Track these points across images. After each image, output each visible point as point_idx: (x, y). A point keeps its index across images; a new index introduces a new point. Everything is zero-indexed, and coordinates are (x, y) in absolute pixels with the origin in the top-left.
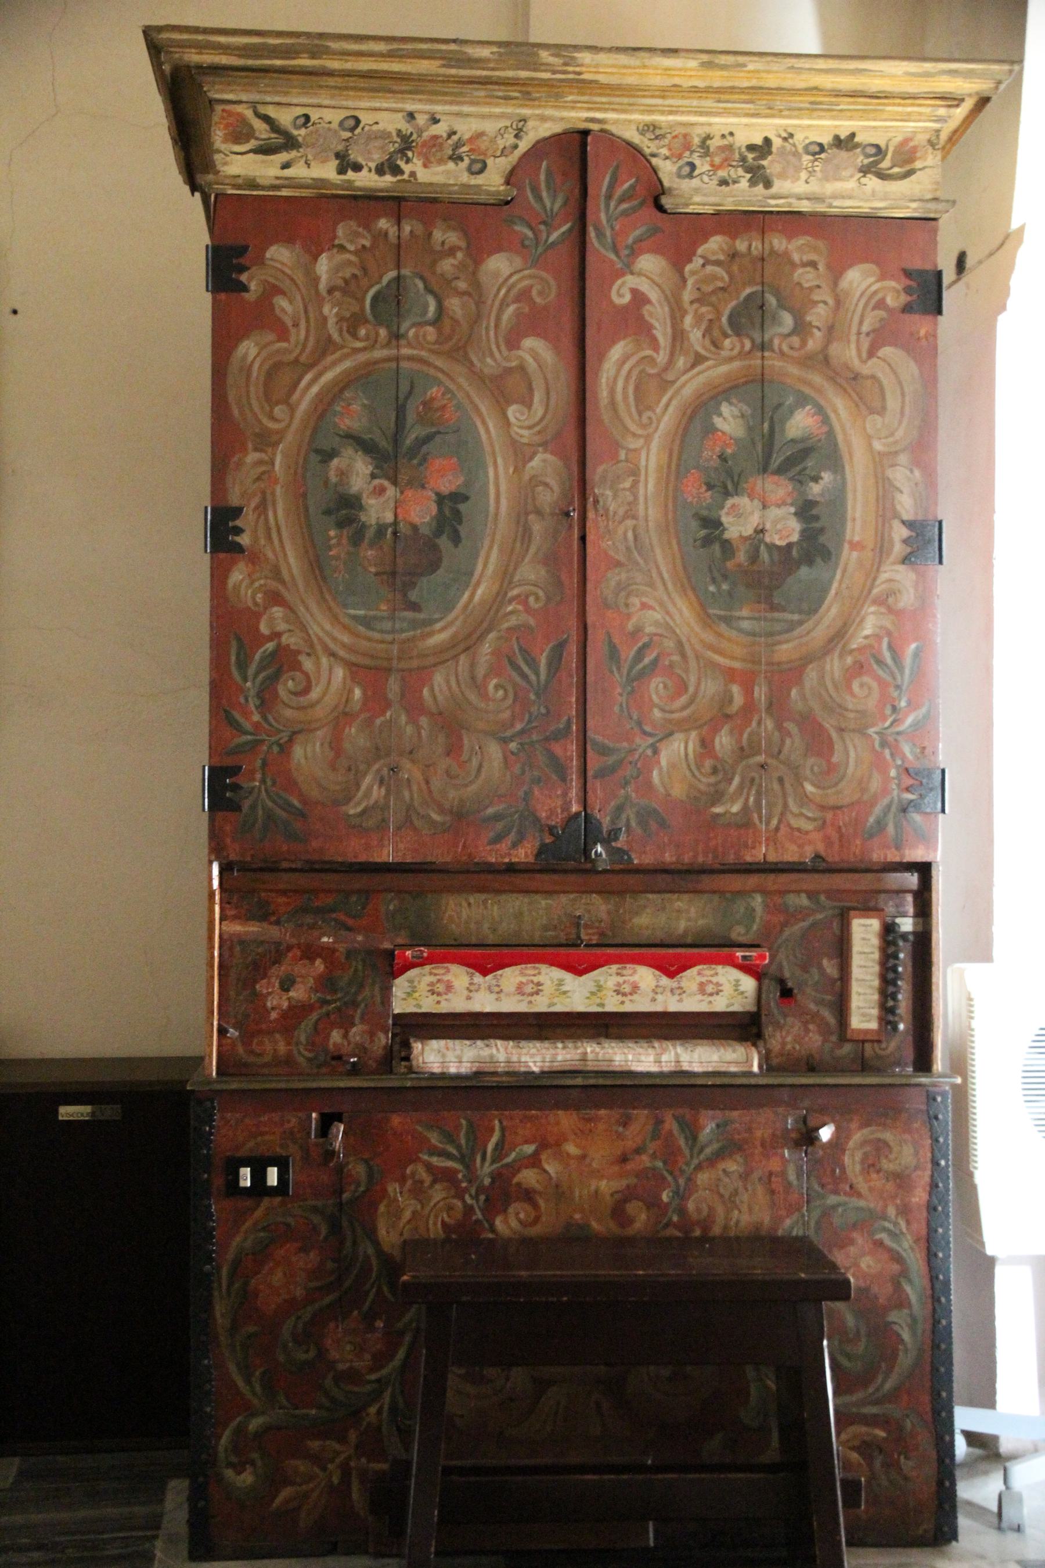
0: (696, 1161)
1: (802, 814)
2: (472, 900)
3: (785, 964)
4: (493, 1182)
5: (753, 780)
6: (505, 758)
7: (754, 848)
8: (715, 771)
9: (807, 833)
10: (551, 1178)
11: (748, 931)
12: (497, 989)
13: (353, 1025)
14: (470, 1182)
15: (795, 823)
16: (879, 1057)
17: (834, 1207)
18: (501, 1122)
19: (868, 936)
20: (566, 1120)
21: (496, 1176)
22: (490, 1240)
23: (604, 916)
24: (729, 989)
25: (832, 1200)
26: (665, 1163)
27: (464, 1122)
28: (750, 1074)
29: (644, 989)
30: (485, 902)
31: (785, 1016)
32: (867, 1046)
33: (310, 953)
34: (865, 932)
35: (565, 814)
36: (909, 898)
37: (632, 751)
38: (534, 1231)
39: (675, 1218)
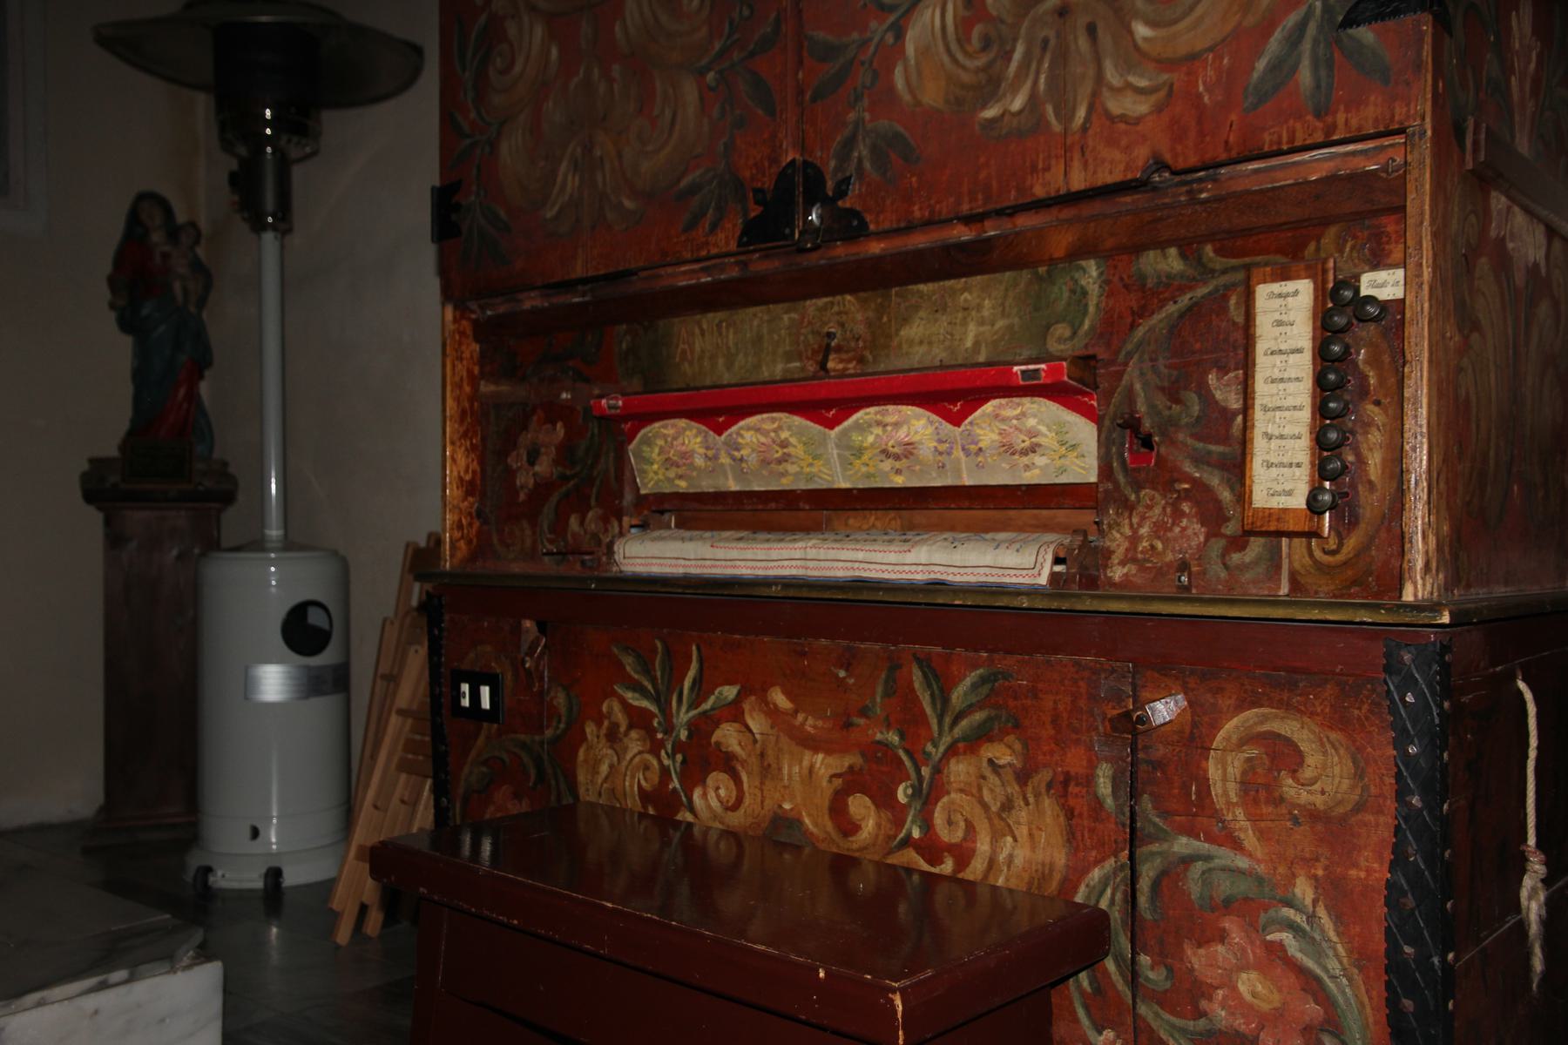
0: (946, 740)
1: (1129, 86)
3: (1138, 386)
4: (690, 736)
5: (1046, 41)
6: (702, 99)
8: (987, 44)
9: (1139, 120)
10: (755, 741)
11: (1074, 333)
13: (589, 508)
14: (665, 733)
15: (1115, 106)
17: (1187, 861)
18: (698, 649)
21: (692, 726)
22: (690, 825)
23: (860, 329)
25: (1183, 845)
26: (902, 737)
27: (659, 644)
30: (719, 326)
31: (1138, 487)
33: (555, 412)
37: (865, 43)
38: (736, 819)
39: (916, 834)
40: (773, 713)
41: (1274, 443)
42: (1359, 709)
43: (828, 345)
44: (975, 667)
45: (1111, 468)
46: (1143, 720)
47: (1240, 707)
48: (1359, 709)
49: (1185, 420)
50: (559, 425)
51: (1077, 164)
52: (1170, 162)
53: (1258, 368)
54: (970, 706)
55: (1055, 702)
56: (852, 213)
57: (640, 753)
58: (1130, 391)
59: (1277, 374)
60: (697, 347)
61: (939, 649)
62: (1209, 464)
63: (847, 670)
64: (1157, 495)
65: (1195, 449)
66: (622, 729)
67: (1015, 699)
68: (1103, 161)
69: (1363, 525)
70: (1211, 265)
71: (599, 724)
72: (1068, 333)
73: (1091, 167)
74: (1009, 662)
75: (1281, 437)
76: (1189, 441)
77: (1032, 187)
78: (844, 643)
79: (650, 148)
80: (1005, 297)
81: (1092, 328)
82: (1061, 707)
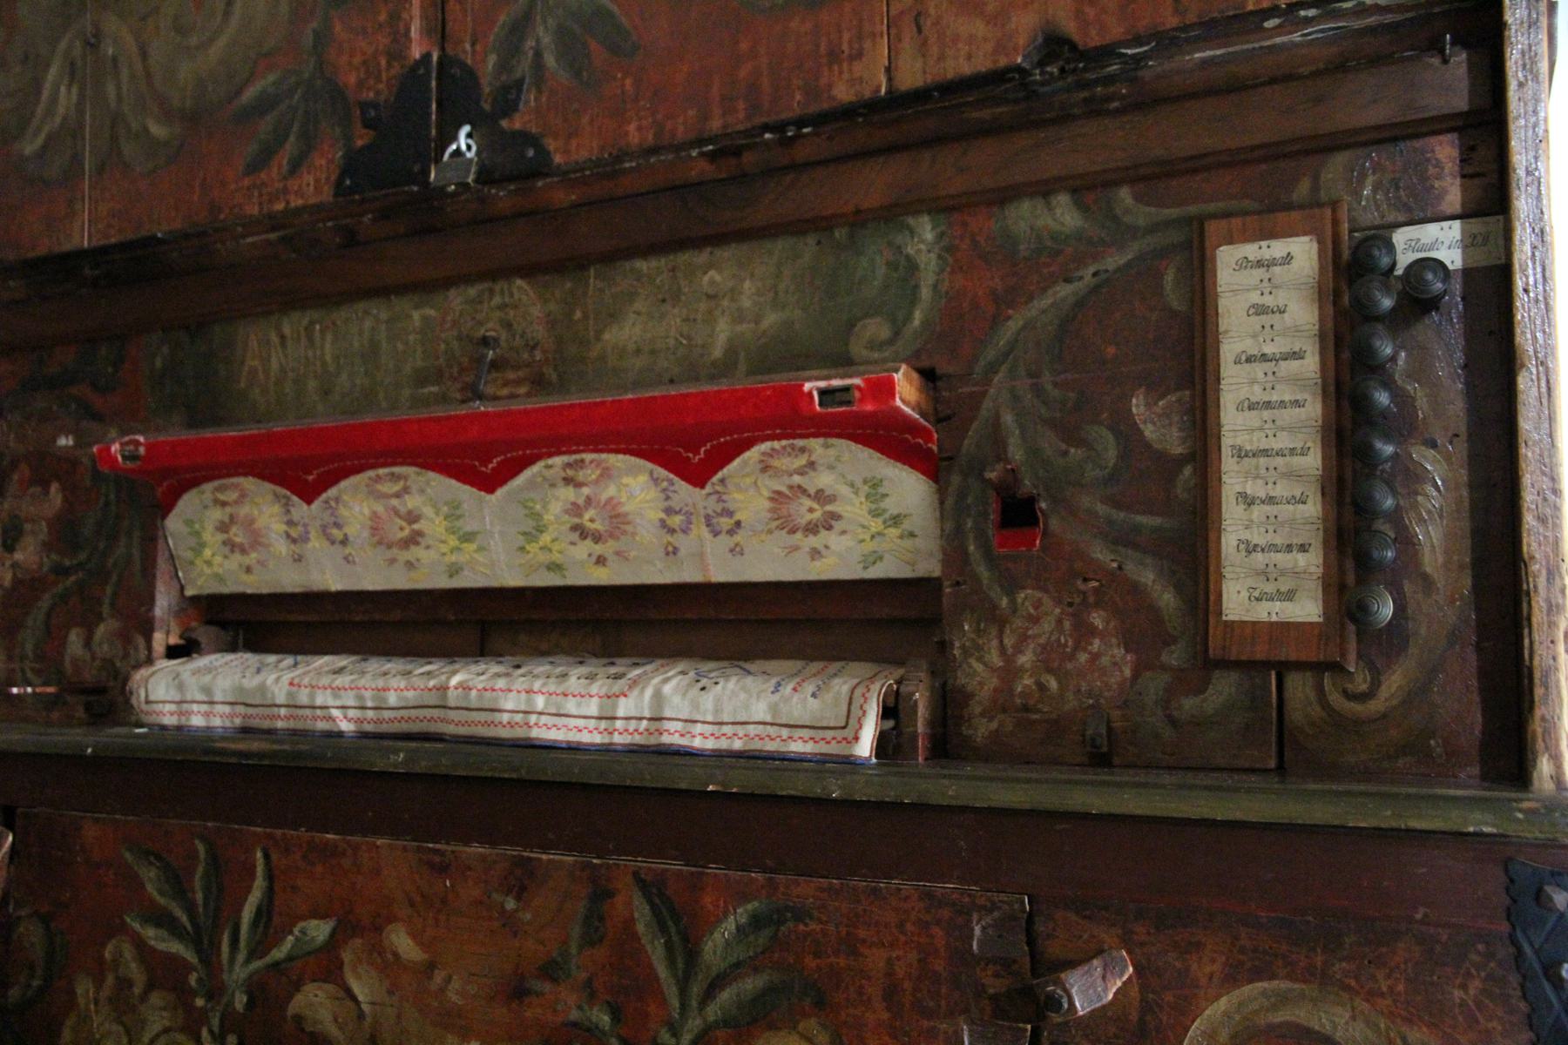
2: (287, 330)
3: (1008, 419)
4: (250, 1005)
7: (859, 55)
10: (361, 1016)
12: (725, 523)
13: (100, 618)
14: (210, 997)
16: (1338, 722)
18: (267, 856)
19: (1280, 298)
20: (390, 860)
21: (256, 990)
23: (539, 332)
24: (859, 516)
26: (616, 1013)
27: (201, 848)
28: (850, 763)
29: (618, 518)
30: (309, 329)
31: (1011, 586)
32: (1299, 688)
33: (47, 468)
34: (1266, 293)
35: (396, 69)
36: (1445, 150)
40: (389, 966)
41: (1257, 512)
42: (1464, 987)
43: (481, 359)
44: (744, 898)
45: (966, 553)
46: (1053, 1003)
47: (1232, 979)
48: (1464, 987)
49: (1092, 473)
50: (54, 487)
51: (907, 46)
52: (1076, 38)
53: (1224, 385)
54: (738, 965)
55: (889, 961)
56: (525, 138)
57: (166, 1031)
58: (996, 423)
59: (1258, 394)
60: (274, 365)
61: (676, 866)
62: (1135, 546)
63: (518, 898)
64: (1046, 600)
65: (1110, 522)
66: (137, 991)
67: (817, 955)
68: (956, 39)
69: (1413, 650)
70: (1127, 219)
71: (99, 982)
72: (885, 333)
73: (935, 50)
74: (806, 890)
75: (1271, 500)
76: (1101, 509)
77: (830, 86)
78: (513, 852)
79: (194, 41)
80: (778, 275)
81: (926, 323)
82: (900, 971)
